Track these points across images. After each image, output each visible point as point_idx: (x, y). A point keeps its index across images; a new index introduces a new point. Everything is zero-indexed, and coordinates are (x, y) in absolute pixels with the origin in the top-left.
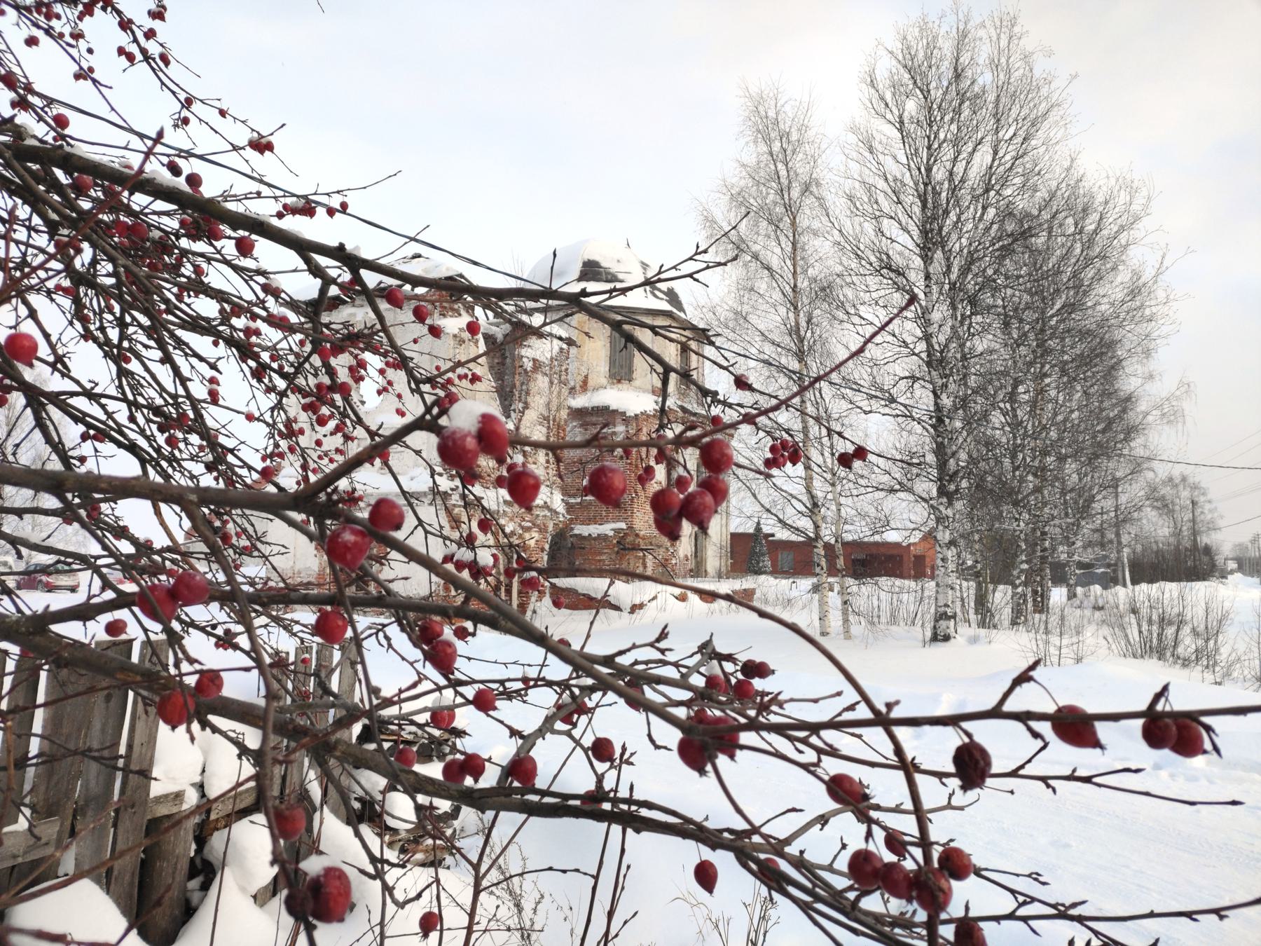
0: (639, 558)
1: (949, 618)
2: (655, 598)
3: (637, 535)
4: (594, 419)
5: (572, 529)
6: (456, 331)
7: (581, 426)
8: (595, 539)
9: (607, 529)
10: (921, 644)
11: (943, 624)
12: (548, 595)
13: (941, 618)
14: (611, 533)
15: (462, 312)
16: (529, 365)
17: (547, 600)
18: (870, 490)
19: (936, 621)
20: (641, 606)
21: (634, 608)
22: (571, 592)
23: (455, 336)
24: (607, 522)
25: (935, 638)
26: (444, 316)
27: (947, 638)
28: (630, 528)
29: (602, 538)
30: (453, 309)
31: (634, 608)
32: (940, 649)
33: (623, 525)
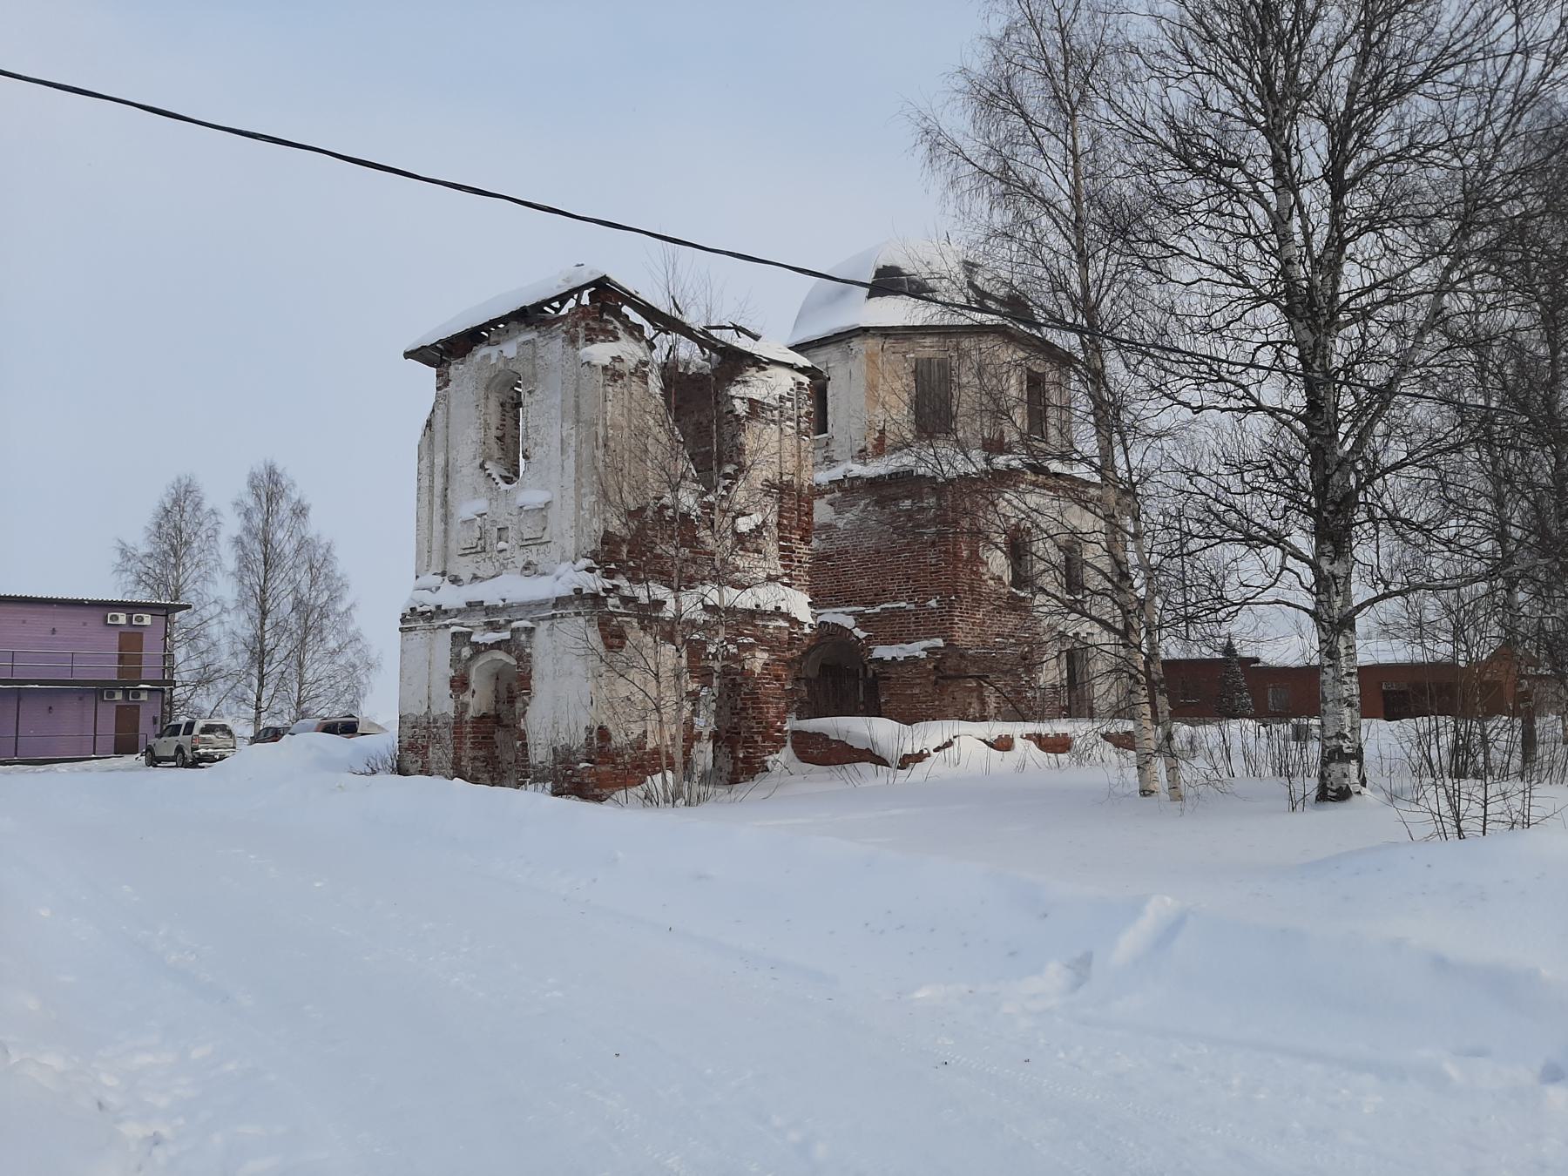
0: (971, 690)
1: (1347, 758)
2: (949, 744)
3: (962, 656)
4: (893, 490)
5: (871, 651)
6: (607, 361)
7: (877, 503)
8: (901, 664)
9: (917, 649)
10: (1286, 804)
11: (1336, 768)
12: (789, 744)
13: (1332, 760)
14: (923, 655)
15: (620, 334)
16: (741, 408)
17: (786, 755)
18: (1213, 541)
19: (1325, 764)
20: (920, 757)
21: (907, 761)
22: (820, 738)
23: (605, 368)
24: (918, 639)
25: (1323, 796)
26: (592, 341)
27: (1343, 795)
28: (950, 644)
29: (912, 661)
30: (605, 331)
31: (907, 761)
32: (1334, 813)
33: (940, 642)
